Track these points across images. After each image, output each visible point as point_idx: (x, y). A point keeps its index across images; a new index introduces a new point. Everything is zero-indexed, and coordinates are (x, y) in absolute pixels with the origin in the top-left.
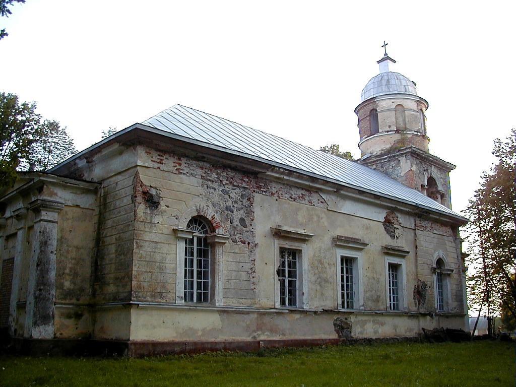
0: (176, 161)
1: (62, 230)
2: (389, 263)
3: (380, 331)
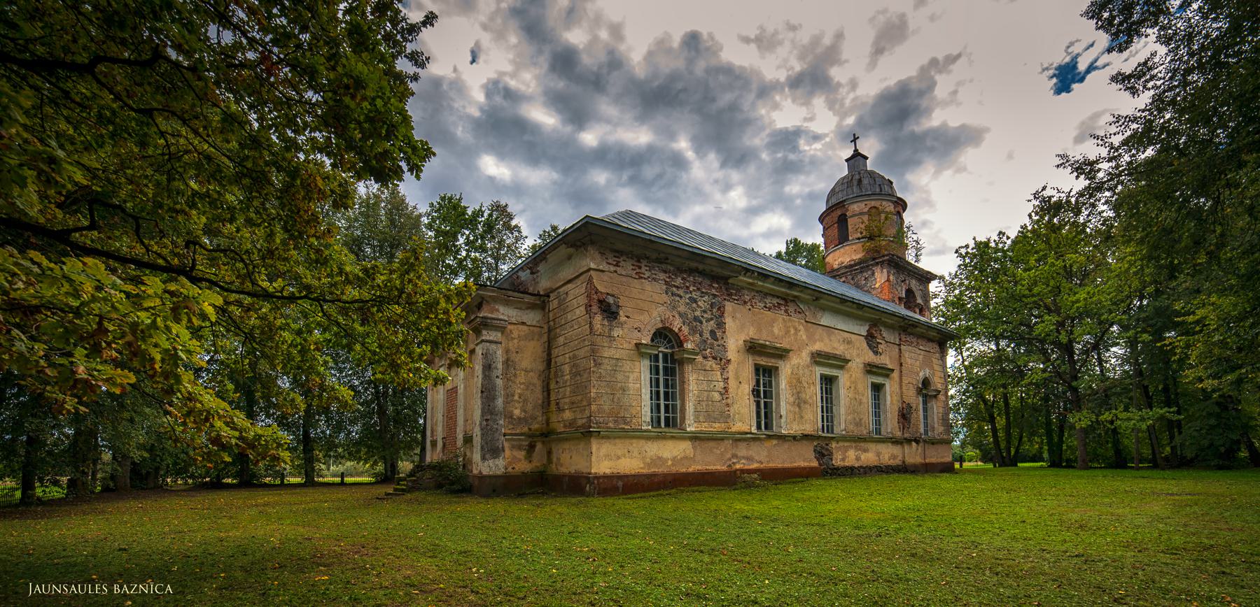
0: (635, 263)
1: (507, 351)
3: (863, 457)
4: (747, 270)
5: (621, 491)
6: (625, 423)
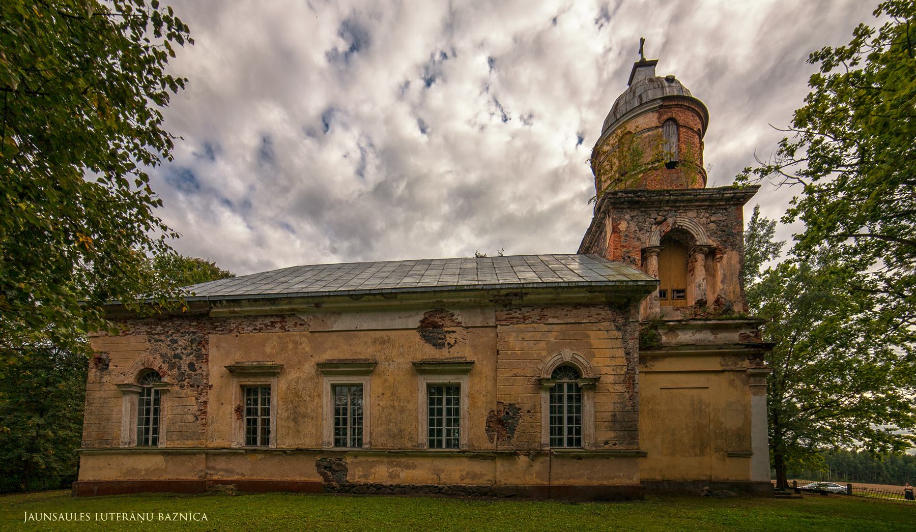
2: (331, 384)
4: (215, 302)
5: (96, 492)
6: (107, 444)
